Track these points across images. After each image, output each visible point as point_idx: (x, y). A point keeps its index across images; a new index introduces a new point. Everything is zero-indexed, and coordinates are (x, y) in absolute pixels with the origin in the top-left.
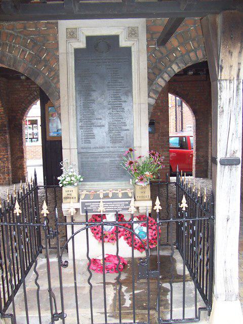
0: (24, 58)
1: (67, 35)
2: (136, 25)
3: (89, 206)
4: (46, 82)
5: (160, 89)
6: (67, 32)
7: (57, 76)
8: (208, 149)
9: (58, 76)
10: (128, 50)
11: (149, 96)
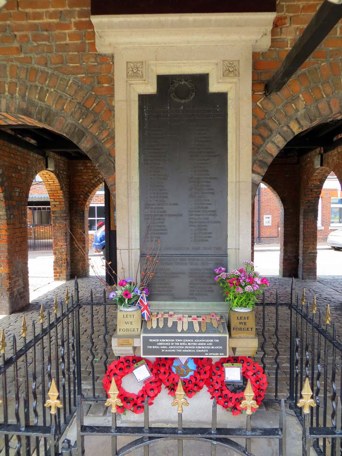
0: (63, 109)
1: (128, 73)
2: (237, 59)
3: (155, 344)
4: (95, 147)
5: (270, 160)
6: (127, 68)
7: (112, 138)
8: (298, 243)
9: (113, 138)
10: (222, 97)
11: (253, 172)
